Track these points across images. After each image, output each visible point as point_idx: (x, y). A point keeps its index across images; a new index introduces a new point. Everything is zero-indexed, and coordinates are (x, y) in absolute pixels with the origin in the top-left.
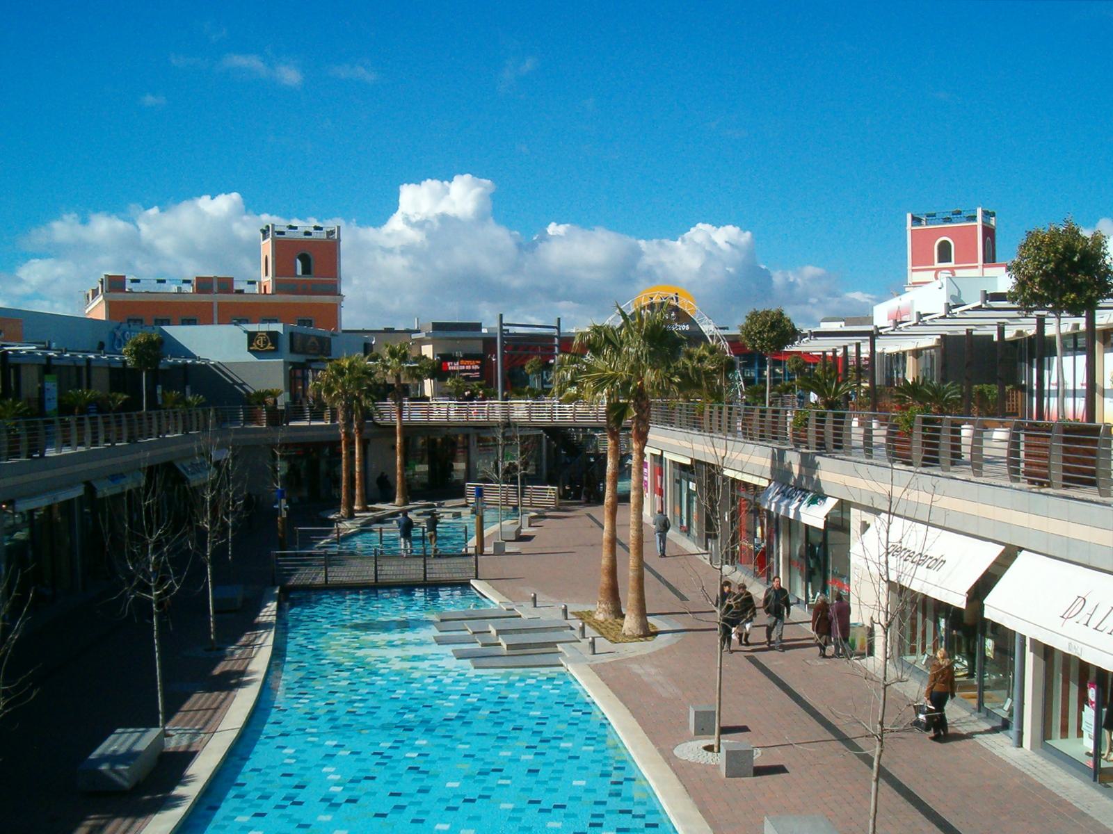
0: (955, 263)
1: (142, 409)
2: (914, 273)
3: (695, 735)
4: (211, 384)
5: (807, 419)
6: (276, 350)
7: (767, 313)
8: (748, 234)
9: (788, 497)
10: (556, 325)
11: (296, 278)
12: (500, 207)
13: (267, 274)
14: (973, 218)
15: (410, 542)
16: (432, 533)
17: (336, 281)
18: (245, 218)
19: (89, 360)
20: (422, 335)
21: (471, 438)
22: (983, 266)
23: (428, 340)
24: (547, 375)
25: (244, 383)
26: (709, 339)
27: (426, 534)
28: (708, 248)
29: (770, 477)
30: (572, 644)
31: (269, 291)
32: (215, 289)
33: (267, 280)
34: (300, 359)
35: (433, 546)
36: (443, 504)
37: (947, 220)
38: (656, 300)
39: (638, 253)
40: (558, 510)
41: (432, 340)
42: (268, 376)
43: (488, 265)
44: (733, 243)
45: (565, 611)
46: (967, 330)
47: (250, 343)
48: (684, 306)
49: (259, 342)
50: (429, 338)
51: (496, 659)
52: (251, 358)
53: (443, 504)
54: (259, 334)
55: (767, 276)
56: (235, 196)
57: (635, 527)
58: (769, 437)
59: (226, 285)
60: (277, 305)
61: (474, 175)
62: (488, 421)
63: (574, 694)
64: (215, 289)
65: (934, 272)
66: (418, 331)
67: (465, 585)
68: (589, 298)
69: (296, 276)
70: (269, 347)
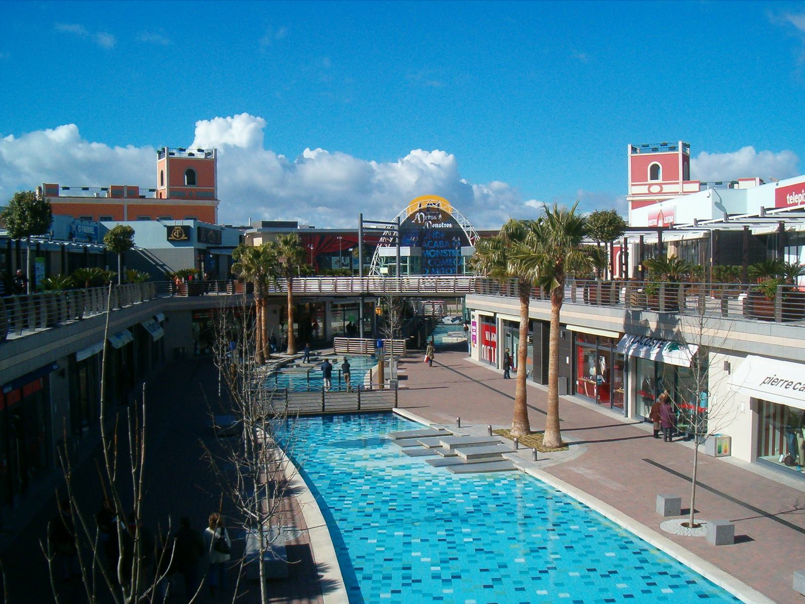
0: (663, 180)
1: (117, 283)
2: (633, 187)
3: (665, 516)
4: (142, 263)
5: (658, 290)
6: (189, 240)
7: (605, 213)
8: (451, 156)
9: (645, 345)
10: (397, 222)
11: (184, 187)
12: (270, 138)
13: (162, 184)
14: (674, 148)
15: (330, 381)
16: (347, 374)
17: (213, 190)
18: (80, 145)
19: (63, 247)
20: (255, 230)
21: (327, 304)
22: (683, 183)
23: (259, 234)
24: (344, 260)
25: (164, 265)
26: (466, 234)
27: (341, 375)
28: (420, 167)
29: (622, 330)
30: (513, 453)
31: (165, 196)
32: (125, 195)
33: (164, 189)
34: (203, 246)
35: (348, 384)
36: (321, 353)
37: (655, 150)
38: (424, 206)
39: (372, 172)
40: (406, 357)
41: (262, 233)
42: (183, 259)
43: (262, 180)
44: (436, 163)
45: (490, 430)
46: (745, 227)
47: (169, 235)
48: (448, 210)
49: (176, 234)
50: (260, 232)
51: (462, 466)
52: (170, 246)
53: (321, 353)
54: (176, 228)
55: (467, 189)
56: (72, 126)
57: (553, 367)
58: (613, 302)
59: (133, 192)
60: (167, 207)
61: (250, 114)
62: (384, 292)
63: (545, 491)
64: (125, 195)
65: (648, 186)
66: (251, 228)
67: (387, 413)
68: (340, 205)
69: (185, 185)
70: (184, 237)
